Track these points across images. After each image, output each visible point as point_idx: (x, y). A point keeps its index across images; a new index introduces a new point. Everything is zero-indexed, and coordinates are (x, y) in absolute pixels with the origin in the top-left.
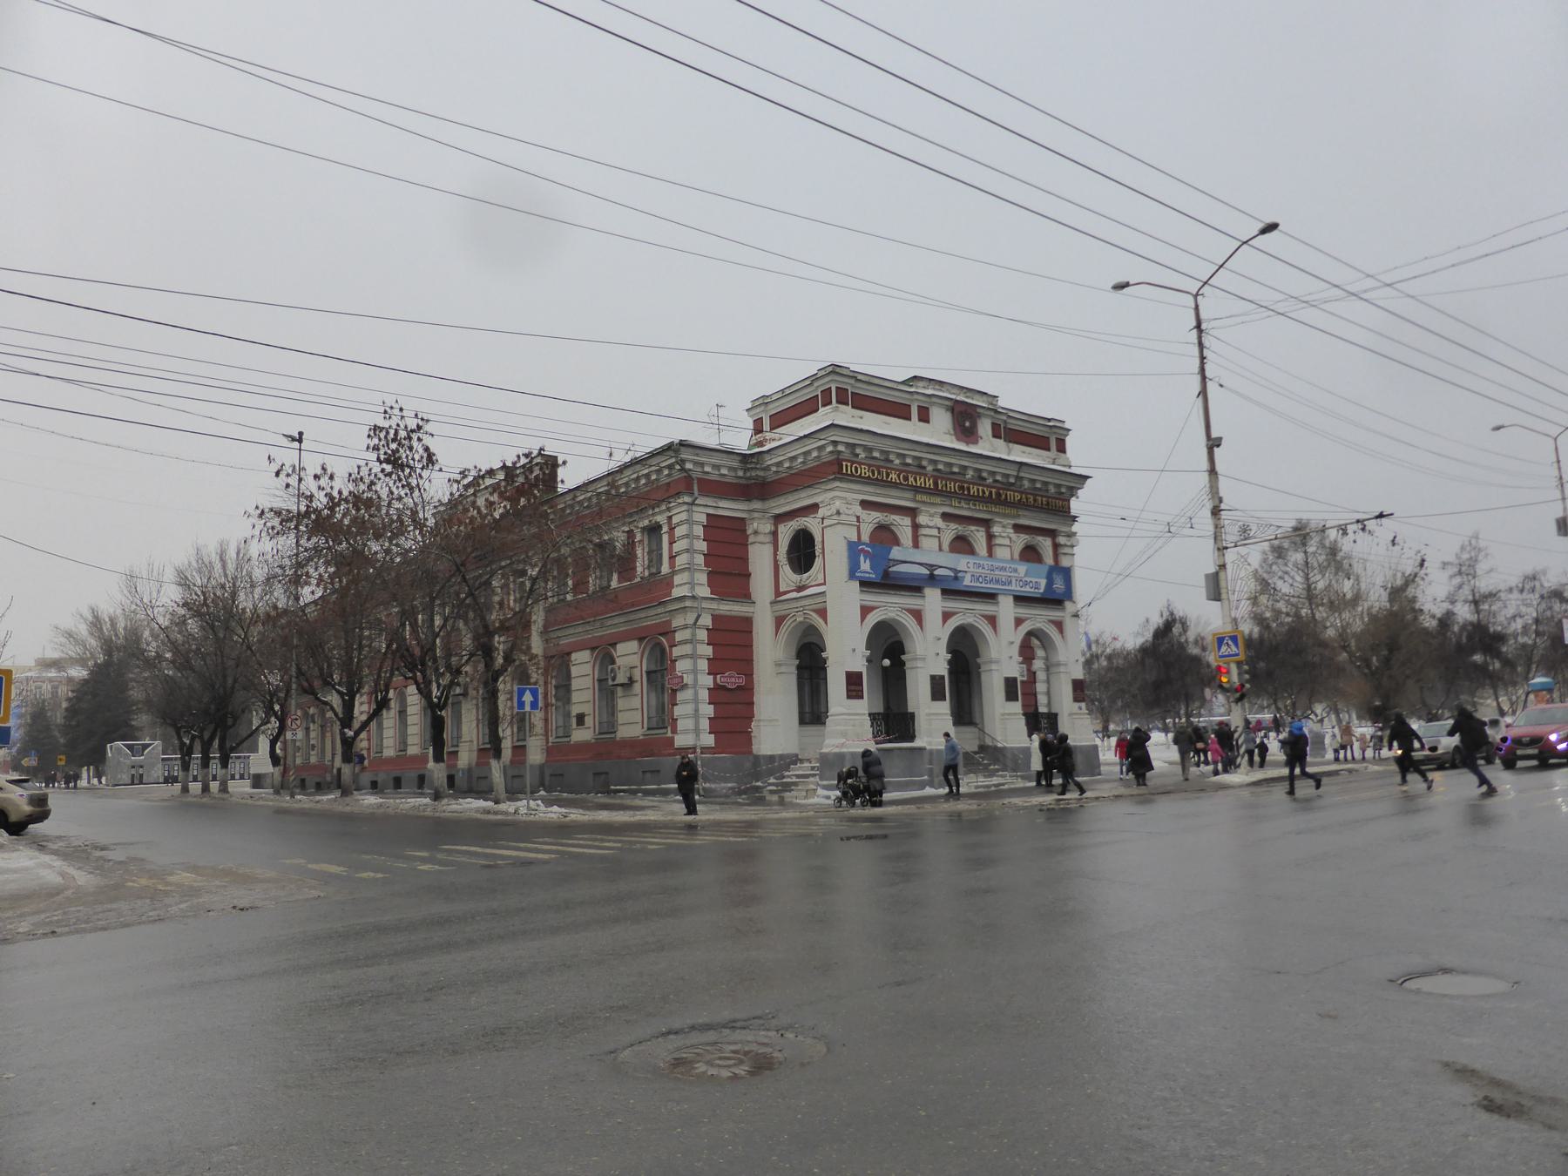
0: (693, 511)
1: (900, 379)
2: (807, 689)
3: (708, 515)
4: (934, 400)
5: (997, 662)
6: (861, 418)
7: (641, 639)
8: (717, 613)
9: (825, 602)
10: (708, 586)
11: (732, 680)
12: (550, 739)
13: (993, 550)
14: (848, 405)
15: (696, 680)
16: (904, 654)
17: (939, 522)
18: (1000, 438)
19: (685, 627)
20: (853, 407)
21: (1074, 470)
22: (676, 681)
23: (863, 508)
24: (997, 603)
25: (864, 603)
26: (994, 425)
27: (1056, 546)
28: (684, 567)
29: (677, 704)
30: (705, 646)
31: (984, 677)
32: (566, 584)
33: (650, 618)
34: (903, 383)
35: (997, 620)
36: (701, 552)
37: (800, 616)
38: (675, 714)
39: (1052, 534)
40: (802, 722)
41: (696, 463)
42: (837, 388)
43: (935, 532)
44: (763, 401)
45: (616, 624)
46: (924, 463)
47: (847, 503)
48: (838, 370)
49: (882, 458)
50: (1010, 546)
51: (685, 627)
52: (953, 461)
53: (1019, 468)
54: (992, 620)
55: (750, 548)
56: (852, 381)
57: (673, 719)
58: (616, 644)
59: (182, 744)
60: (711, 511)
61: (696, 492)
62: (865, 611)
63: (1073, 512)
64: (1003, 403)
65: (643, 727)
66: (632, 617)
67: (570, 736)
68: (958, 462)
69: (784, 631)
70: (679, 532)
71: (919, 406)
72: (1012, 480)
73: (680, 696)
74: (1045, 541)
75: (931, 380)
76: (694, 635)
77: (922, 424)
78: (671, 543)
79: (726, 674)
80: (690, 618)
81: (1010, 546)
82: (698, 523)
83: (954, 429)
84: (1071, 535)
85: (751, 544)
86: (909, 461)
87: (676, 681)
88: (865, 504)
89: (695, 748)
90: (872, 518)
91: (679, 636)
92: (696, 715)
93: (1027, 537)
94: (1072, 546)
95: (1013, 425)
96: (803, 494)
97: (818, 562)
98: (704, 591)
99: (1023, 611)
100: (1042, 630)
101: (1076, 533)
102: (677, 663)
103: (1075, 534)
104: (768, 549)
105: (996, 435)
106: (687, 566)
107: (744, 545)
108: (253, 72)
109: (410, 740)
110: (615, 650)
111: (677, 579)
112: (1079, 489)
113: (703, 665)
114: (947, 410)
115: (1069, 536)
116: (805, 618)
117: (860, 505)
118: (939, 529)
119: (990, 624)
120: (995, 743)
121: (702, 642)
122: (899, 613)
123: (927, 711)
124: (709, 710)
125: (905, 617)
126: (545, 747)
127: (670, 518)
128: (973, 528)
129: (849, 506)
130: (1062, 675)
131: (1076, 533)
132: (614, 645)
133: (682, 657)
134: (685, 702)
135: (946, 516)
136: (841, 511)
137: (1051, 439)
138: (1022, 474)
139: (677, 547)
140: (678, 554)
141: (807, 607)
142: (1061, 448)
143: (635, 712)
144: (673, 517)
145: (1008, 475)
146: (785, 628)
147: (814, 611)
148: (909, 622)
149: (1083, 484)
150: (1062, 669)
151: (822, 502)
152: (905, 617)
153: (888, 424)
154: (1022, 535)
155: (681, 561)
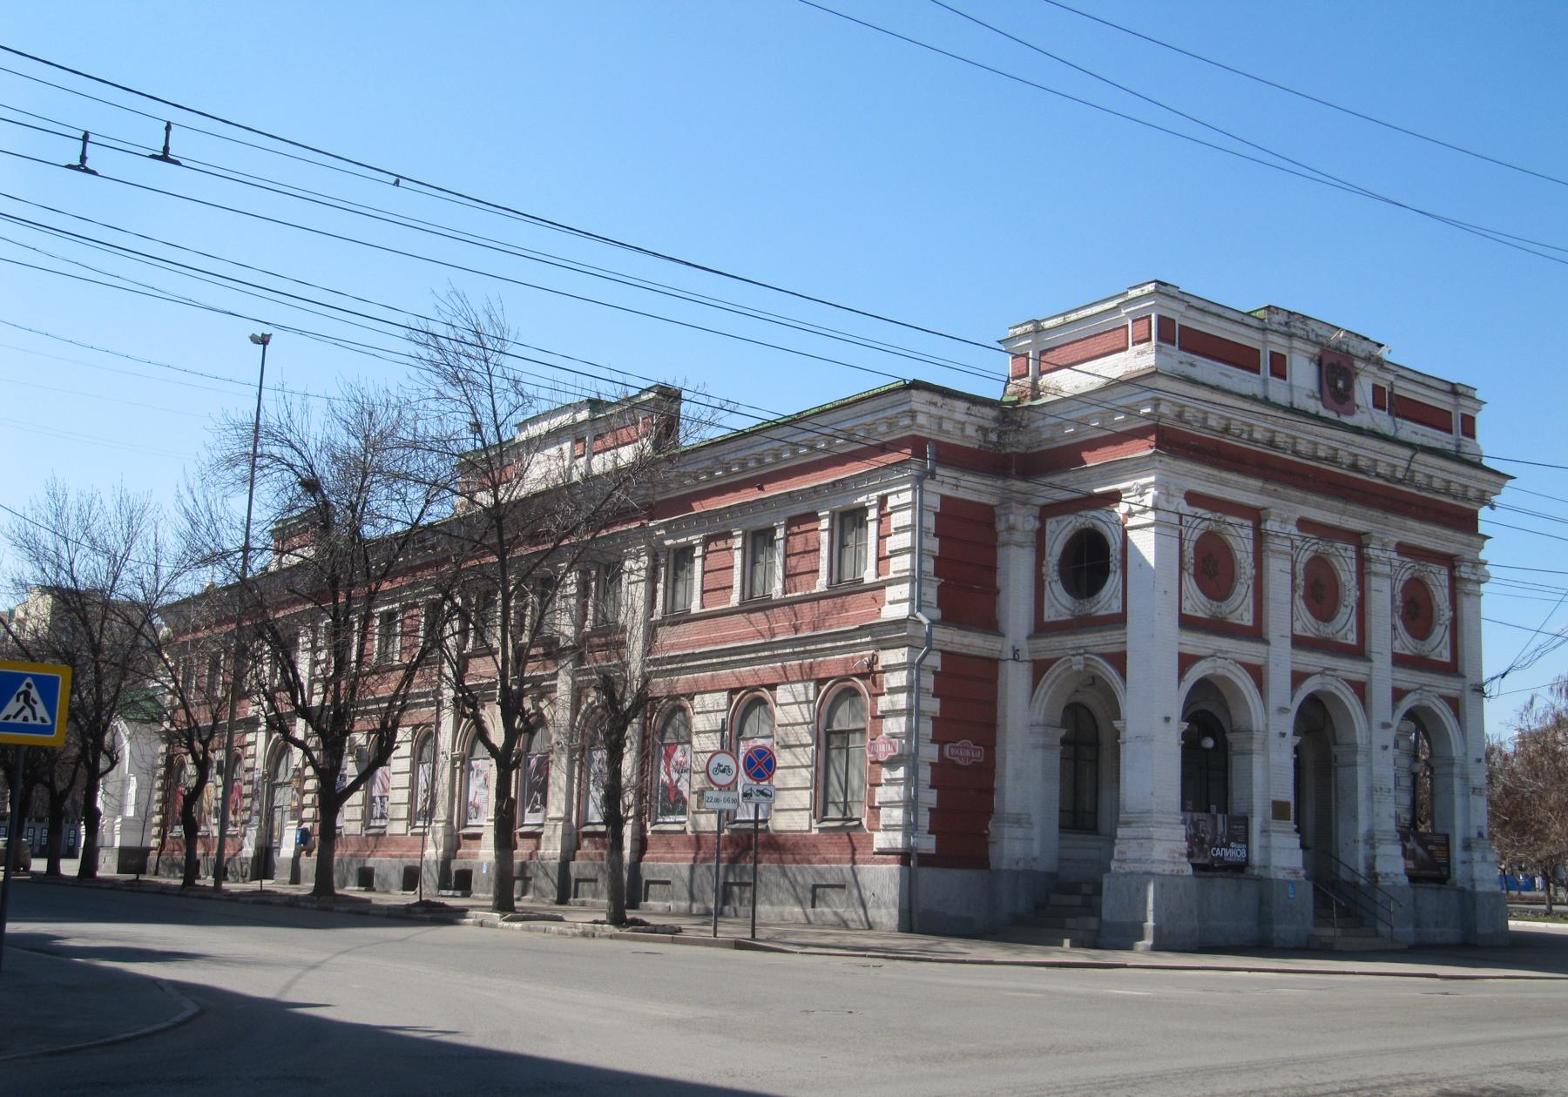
11: (965, 753)
18: (1384, 409)
20: (1182, 348)
23: (1400, 554)
25: (1295, 665)
27: (1454, 581)
32: (590, 574)
35: (1366, 688)
39: (1450, 561)
55: (1001, 553)
59: (1431, 843)
62: (1186, 661)
63: (1483, 528)
74: (1346, 550)
78: (881, 538)
84: (1478, 564)
100: (1429, 708)
105: (1378, 404)
108: (1282, 160)
114: (1311, 360)
126: (639, 837)
144: (889, 498)
147: (1102, 655)
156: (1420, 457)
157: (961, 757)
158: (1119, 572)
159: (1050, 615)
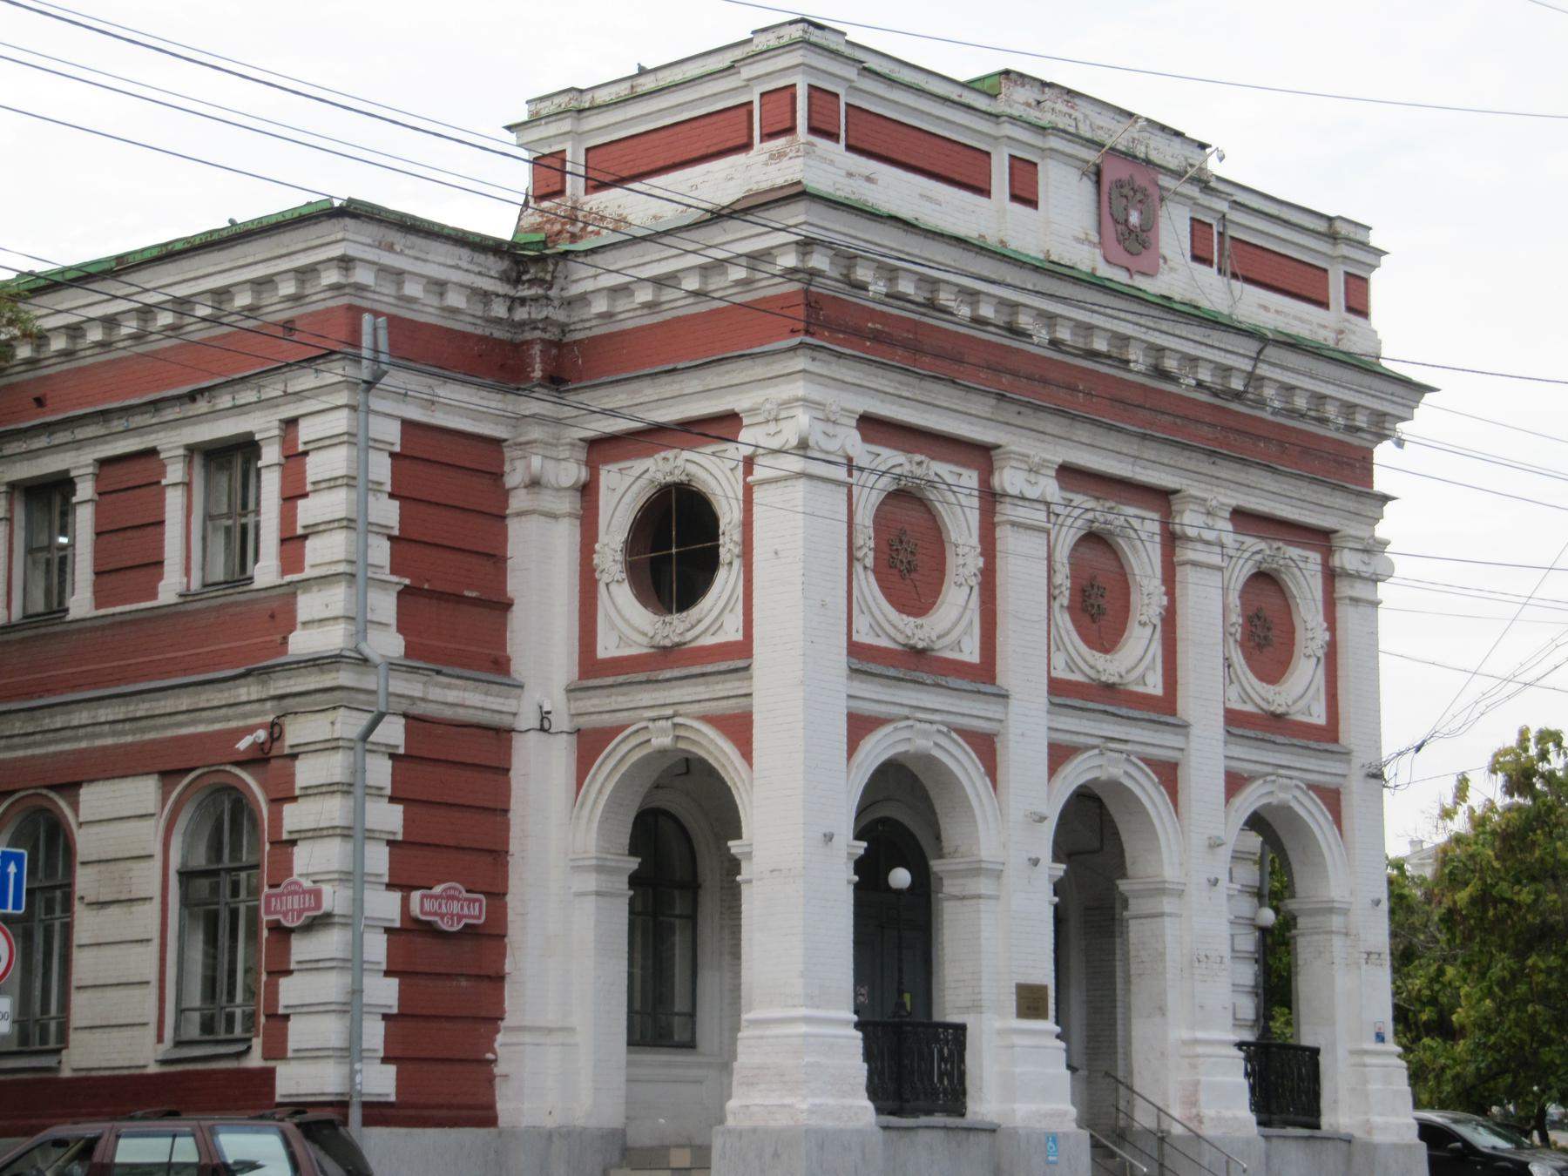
0: (369, 411)
1: (963, 77)
2: (638, 939)
4: (1054, 142)
5: (1180, 894)
7: (168, 776)
8: (420, 709)
13: (1178, 577)
14: (837, 141)
16: (1124, 876)
17: (1049, 488)
19: (332, 745)
23: (1064, 486)
26: (1198, 228)
27: (1331, 576)
29: (289, 972)
30: (384, 804)
31: (1136, 931)
34: (968, 85)
35: (1180, 773)
37: (663, 731)
39: (1321, 538)
40: (632, 1043)
46: (1024, 321)
48: (816, 37)
49: (920, 299)
51: (332, 745)
52: (1096, 320)
55: (515, 529)
56: (851, 73)
57: (272, 1016)
60: (415, 414)
62: (860, 726)
63: (1381, 483)
65: (160, 1039)
66: (142, 708)
72: (1237, 384)
73: (301, 949)
75: (1044, 84)
77: (1018, 208)
78: (292, 495)
79: (438, 890)
84: (1374, 548)
85: (520, 514)
86: (987, 311)
87: (295, 902)
88: (872, 426)
92: (351, 1007)
93: (1262, 545)
94: (1375, 580)
96: (692, 383)
97: (726, 581)
98: (388, 644)
99: (1250, 756)
100: (1290, 809)
101: (1385, 543)
102: (296, 849)
104: (565, 536)
106: (342, 568)
110: (75, 807)
111: (308, 605)
112: (1403, 419)
116: (677, 738)
117: (858, 427)
118: (1048, 504)
121: (375, 792)
122: (1298, 794)
123: (1186, 1034)
127: (291, 423)
128: (1294, 552)
129: (831, 429)
132: (70, 788)
133: (317, 834)
134: (314, 966)
135: (1070, 474)
136: (811, 443)
137: (1331, 275)
138: (1263, 370)
139: (308, 511)
140: (313, 531)
141: (682, 709)
142: (1358, 307)
143: (137, 992)
144: (302, 424)
145: (1229, 369)
147: (708, 719)
148: (963, 764)
150: (1336, 922)
151: (752, 411)
155: (323, 552)
156: (1272, 353)
157: (442, 916)
158: (737, 563)
159: (607, 647)
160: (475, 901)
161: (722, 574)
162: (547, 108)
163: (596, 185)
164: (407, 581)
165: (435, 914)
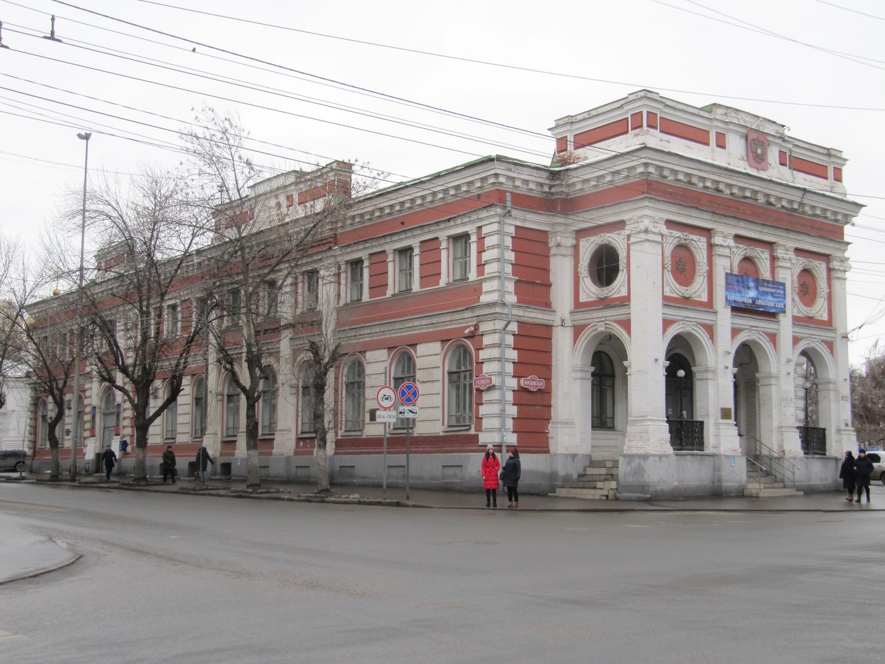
3: (517, 227)
6: (668, 141)
8: (522, 319)
9: (630, 313)
10: (516, 294)
11: (533, 383)
12: (340, 433)
15: (503, 381)
18: (655, 128)
19: (494, 332)
20: (661, 131)
21: (849, 198)
22: (483, 382)
23: (668, 228)
24: (778, 322)
26: (782, 154)
28: (494, 275)
29: (482, 404)
33: (449, 322)
35: (777, 337)
36: (509, 262)
37: (602, 326)
38: (480, 414)
39: (826, 257)
41: (508, 177)
42: (648, 112)
43: (659, 239)
44: (570, 121)
45: (421, 325)
47: (724, 237)
48: (649, 95)
50: (730, 257)
51: (494, 332)
53: (804, 195)
54: (773, 338)
55: (552, 260)
56: (661, 107)
57: (477, 418)
58: (416, 345)
61: (509, 204)
62: (667, 323)
64: (792, 132)
65: (443, 424)
66: (435, 320)
67: (361, 431)
68: (751, 187)
69: (583, 339)
70: (488, 242)
71: (717, 133)
76: (502, 339)
77: (719, 149)
78: (480, 251)
79: (529, 378)
80: (499, 325)
81: (730, 257)
82: (507, 234)
83: (747, 156)
84: (844, 260)
87: (483, 382)
89: (500, 446)
90: (742, 251)
91: (486, 340)
94: (845, 271)
95: (799, 153)
96: (609, 211)
97: (621, 277)
98: (512, 299)
99: (801, 331)
103: (847, 259)
106: (497, 274)
107: (546, 256)
109: (180, 429)
111: (486, 287)
113: (510, 368)
114: (742, 137)
115: (842, 261)
118: (662, 235)
119: (771, 340)
120: (772, 453)
121: (508, 346)
124: (513, 411)
125: (699, 331)
127: (480, 228)
128: (694, 237)
130: (710, 382)
131: (849, 259)
132: (414, 345)
133: (490, 360)
134: (490, 402)
138: (805, 201)
139: (485, 256)
140: (487, 262)
141: (608, 318)
142: (838, 178)
143: (436, 410)
144: (483, 228)
146: (585, 336)
147: (616, 321)
148: (702, 336)
149: (857, 213)
150: (832, 386)
151: (630, 220)
152: (699, 331)
153: (691, 148)
154: (801, 259)
155: (489, 269)
157: (530, 386)
158: (625, 270)
159: (583, 298)
160: (541, 381)
161: (620, 274)
162: (561, 122)
163: (576, 148)
164: (517, 278)
165: (528, 385)
